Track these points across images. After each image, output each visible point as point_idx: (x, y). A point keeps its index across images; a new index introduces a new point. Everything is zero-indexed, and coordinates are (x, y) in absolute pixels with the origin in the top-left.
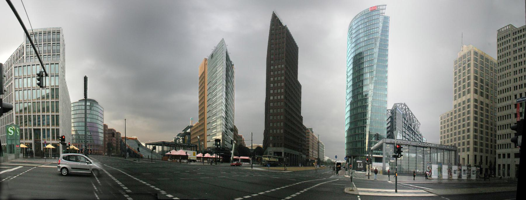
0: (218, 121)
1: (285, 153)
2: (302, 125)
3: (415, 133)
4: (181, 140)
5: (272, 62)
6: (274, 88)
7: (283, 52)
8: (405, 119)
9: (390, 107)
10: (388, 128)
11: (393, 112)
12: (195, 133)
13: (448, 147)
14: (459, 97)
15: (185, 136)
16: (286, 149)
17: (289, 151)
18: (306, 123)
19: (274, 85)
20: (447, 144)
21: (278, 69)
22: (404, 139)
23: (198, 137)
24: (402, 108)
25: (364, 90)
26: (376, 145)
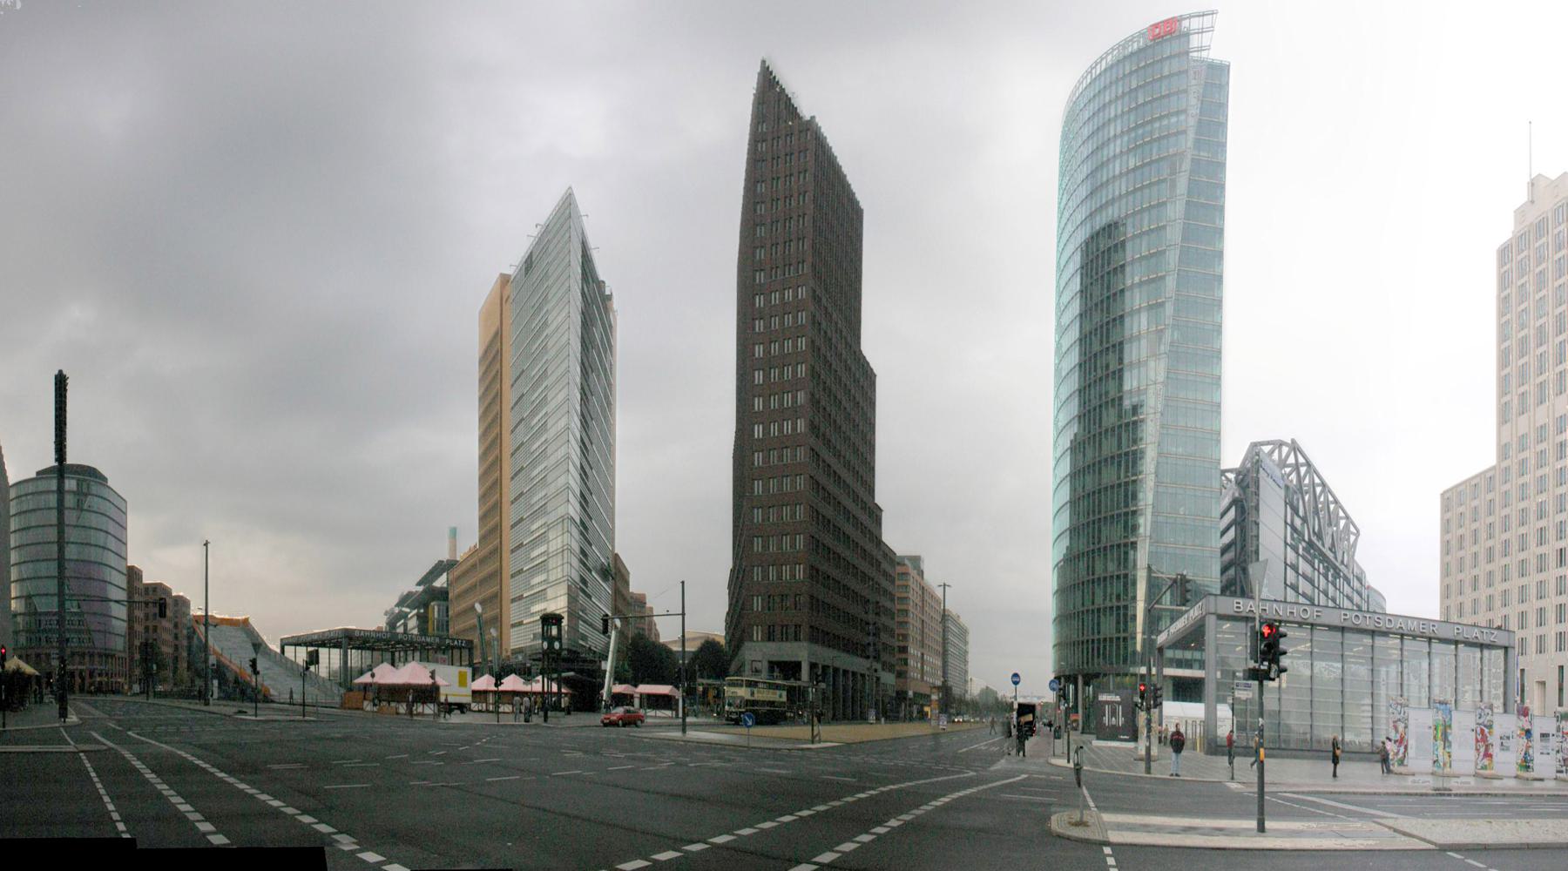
0: (551, 535)
1: (813, 666)
2: (878, 542)
7: (801, 229)
8: (1295, 511)
9: (1232, 457)
10: (1224, 551)
11: (1248, 479)
15: (426, 606)
16: (818, 648)
17: (827, 656)
18: (896, 536)
21: (785, 308)
22: (1291, 594)
23: (478, 607)
24: (1283, 464)
25: (1126, 387)
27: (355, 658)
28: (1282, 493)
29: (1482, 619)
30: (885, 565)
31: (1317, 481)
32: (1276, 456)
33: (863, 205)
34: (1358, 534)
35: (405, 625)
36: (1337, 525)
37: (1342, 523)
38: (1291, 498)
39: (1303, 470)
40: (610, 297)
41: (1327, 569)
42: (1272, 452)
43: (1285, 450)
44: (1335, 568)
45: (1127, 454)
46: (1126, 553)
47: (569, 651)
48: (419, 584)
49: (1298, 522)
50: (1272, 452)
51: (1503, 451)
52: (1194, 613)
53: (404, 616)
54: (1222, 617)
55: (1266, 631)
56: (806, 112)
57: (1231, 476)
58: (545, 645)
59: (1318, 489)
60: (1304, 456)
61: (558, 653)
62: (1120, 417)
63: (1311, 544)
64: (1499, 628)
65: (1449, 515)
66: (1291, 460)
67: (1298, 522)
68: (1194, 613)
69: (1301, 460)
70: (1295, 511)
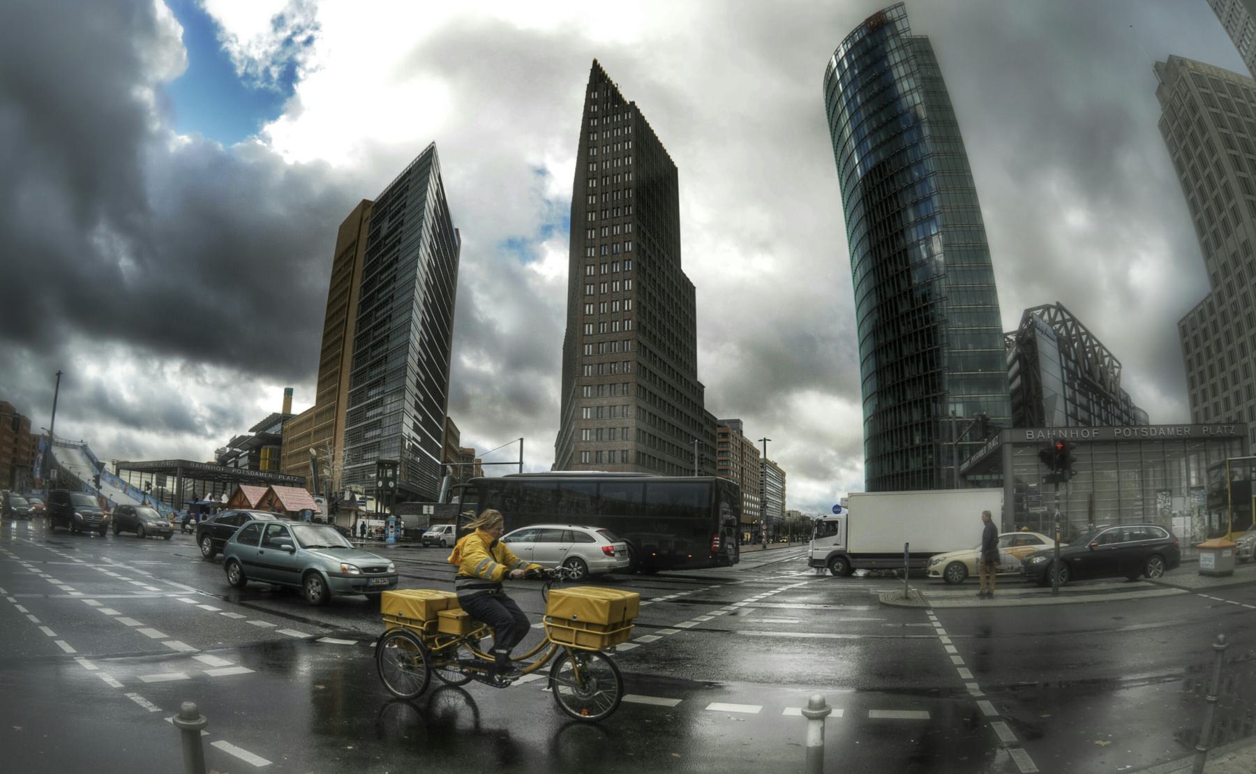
0: (388, 400)
3: (1108, 402)
4: (244, 461)
5: (592, 217)
6: (597, 280)
8: (1068, 357)
11: (1027, 339)
12: (300, 438)
13: (1219, 430)
14: (1234, 256)
15: (258, 449)
19: (597, 309)
20: (1216, 419)
23: (313, 451)
24: (1052, 322)
25: (916, 281)
26: (981, 453)
27: (189, 485)
28: (1055, 344)
29: (1223, 417)
30: (706, 427)
31: (1082, 330)
32: (1046, 317)
33: (677, 164)
34: (1120, 367)
35: (236, 463)
36: (1103, 362)
37: (1107, 360)
38: (1064, 344)
39: (1069, 324)
40: (633, 103)
41: (1099, 398)
42: (1042, 314)
43: (1053, 311)
44: (1106, 396)
45: (922, 331)
46: (928, 406)
47: (401, 490)
48: (251, 430)
49: (1071, 365)
50: (1042, 314)
51: (1214, 279)
52: (993, 444)
53: (237, 455)
54: (1017, 445)
55: (1060, 446)
56: (628, 98)
57: (1012, 337)
58: (380, 484)
59: (1084, 337)
60: (1068, 313)
61: (392, 490)
62: (913, 305)
63: (1084, 381)
64: (1235, 423)
65: (1187, 339)
66: (1059, 318)
67: (1071, 365)
68: (993, 444)
69: (1067, 317)
70: (1068, 357)
